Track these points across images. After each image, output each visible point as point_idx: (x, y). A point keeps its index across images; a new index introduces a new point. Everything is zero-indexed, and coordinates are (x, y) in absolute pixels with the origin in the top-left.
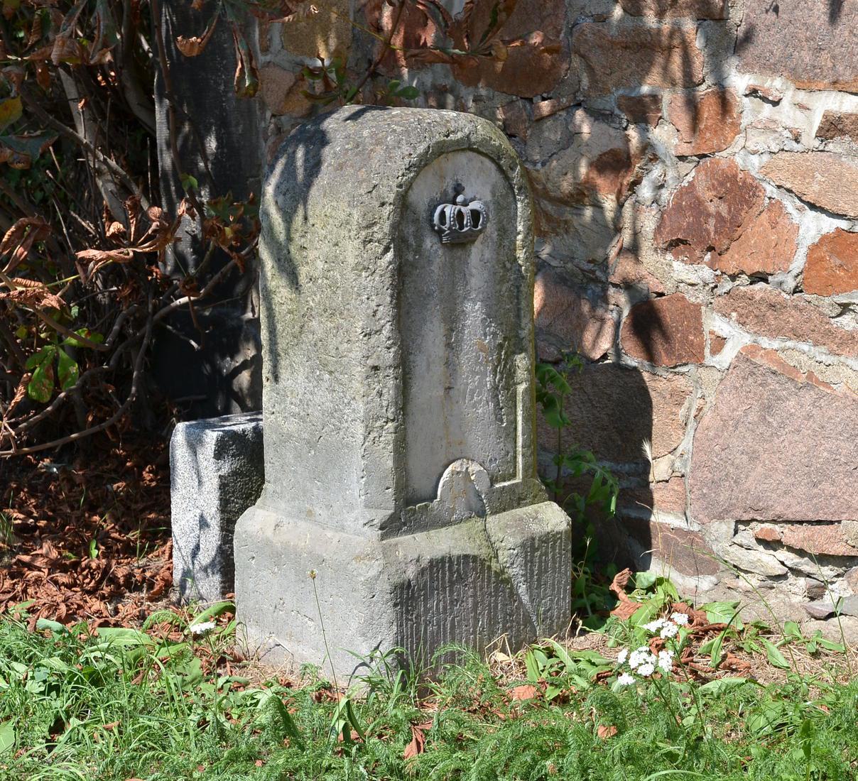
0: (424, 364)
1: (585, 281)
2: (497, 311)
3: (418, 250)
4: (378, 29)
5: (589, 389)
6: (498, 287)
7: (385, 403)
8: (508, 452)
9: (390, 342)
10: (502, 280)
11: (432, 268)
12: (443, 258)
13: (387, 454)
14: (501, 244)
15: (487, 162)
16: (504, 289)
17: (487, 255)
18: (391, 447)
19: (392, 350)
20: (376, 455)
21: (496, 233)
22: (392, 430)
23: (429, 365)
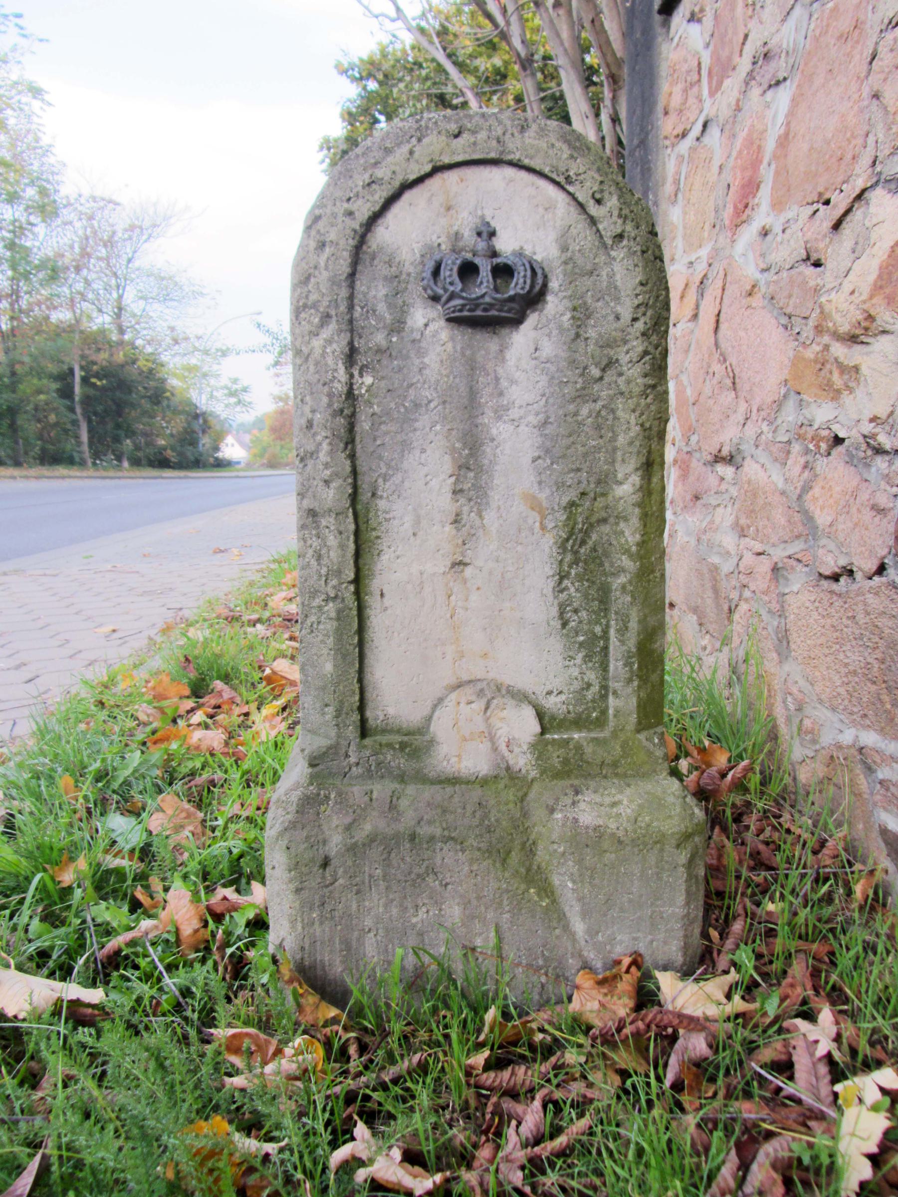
0: (408, 521)
1: (869, 452)
2: (568, 448)
3: (398, 326)
4: (781, 203)
5: (861, 619)
6: (572, 407)
7: (324, 571)
8: (589, 685)
9: (328, 472)
10: (582, 396)
11: (426, 360)
12: (449, 346)
13: (325, 651)
14: (578, 335)
15: (551, 190)
16: (585, 411)
17: (548, 349)
18: (330, 641)
19: (333, 485)
20: (314, 651)
21: (568, 315)
22: (333, 614)
23: (418, 521)
